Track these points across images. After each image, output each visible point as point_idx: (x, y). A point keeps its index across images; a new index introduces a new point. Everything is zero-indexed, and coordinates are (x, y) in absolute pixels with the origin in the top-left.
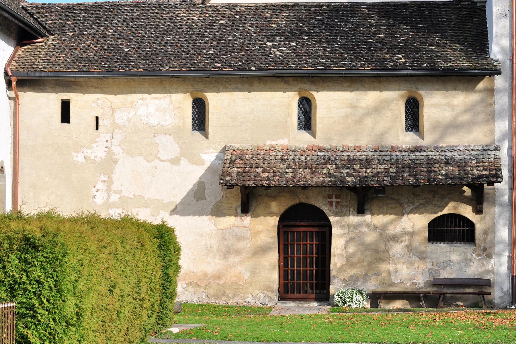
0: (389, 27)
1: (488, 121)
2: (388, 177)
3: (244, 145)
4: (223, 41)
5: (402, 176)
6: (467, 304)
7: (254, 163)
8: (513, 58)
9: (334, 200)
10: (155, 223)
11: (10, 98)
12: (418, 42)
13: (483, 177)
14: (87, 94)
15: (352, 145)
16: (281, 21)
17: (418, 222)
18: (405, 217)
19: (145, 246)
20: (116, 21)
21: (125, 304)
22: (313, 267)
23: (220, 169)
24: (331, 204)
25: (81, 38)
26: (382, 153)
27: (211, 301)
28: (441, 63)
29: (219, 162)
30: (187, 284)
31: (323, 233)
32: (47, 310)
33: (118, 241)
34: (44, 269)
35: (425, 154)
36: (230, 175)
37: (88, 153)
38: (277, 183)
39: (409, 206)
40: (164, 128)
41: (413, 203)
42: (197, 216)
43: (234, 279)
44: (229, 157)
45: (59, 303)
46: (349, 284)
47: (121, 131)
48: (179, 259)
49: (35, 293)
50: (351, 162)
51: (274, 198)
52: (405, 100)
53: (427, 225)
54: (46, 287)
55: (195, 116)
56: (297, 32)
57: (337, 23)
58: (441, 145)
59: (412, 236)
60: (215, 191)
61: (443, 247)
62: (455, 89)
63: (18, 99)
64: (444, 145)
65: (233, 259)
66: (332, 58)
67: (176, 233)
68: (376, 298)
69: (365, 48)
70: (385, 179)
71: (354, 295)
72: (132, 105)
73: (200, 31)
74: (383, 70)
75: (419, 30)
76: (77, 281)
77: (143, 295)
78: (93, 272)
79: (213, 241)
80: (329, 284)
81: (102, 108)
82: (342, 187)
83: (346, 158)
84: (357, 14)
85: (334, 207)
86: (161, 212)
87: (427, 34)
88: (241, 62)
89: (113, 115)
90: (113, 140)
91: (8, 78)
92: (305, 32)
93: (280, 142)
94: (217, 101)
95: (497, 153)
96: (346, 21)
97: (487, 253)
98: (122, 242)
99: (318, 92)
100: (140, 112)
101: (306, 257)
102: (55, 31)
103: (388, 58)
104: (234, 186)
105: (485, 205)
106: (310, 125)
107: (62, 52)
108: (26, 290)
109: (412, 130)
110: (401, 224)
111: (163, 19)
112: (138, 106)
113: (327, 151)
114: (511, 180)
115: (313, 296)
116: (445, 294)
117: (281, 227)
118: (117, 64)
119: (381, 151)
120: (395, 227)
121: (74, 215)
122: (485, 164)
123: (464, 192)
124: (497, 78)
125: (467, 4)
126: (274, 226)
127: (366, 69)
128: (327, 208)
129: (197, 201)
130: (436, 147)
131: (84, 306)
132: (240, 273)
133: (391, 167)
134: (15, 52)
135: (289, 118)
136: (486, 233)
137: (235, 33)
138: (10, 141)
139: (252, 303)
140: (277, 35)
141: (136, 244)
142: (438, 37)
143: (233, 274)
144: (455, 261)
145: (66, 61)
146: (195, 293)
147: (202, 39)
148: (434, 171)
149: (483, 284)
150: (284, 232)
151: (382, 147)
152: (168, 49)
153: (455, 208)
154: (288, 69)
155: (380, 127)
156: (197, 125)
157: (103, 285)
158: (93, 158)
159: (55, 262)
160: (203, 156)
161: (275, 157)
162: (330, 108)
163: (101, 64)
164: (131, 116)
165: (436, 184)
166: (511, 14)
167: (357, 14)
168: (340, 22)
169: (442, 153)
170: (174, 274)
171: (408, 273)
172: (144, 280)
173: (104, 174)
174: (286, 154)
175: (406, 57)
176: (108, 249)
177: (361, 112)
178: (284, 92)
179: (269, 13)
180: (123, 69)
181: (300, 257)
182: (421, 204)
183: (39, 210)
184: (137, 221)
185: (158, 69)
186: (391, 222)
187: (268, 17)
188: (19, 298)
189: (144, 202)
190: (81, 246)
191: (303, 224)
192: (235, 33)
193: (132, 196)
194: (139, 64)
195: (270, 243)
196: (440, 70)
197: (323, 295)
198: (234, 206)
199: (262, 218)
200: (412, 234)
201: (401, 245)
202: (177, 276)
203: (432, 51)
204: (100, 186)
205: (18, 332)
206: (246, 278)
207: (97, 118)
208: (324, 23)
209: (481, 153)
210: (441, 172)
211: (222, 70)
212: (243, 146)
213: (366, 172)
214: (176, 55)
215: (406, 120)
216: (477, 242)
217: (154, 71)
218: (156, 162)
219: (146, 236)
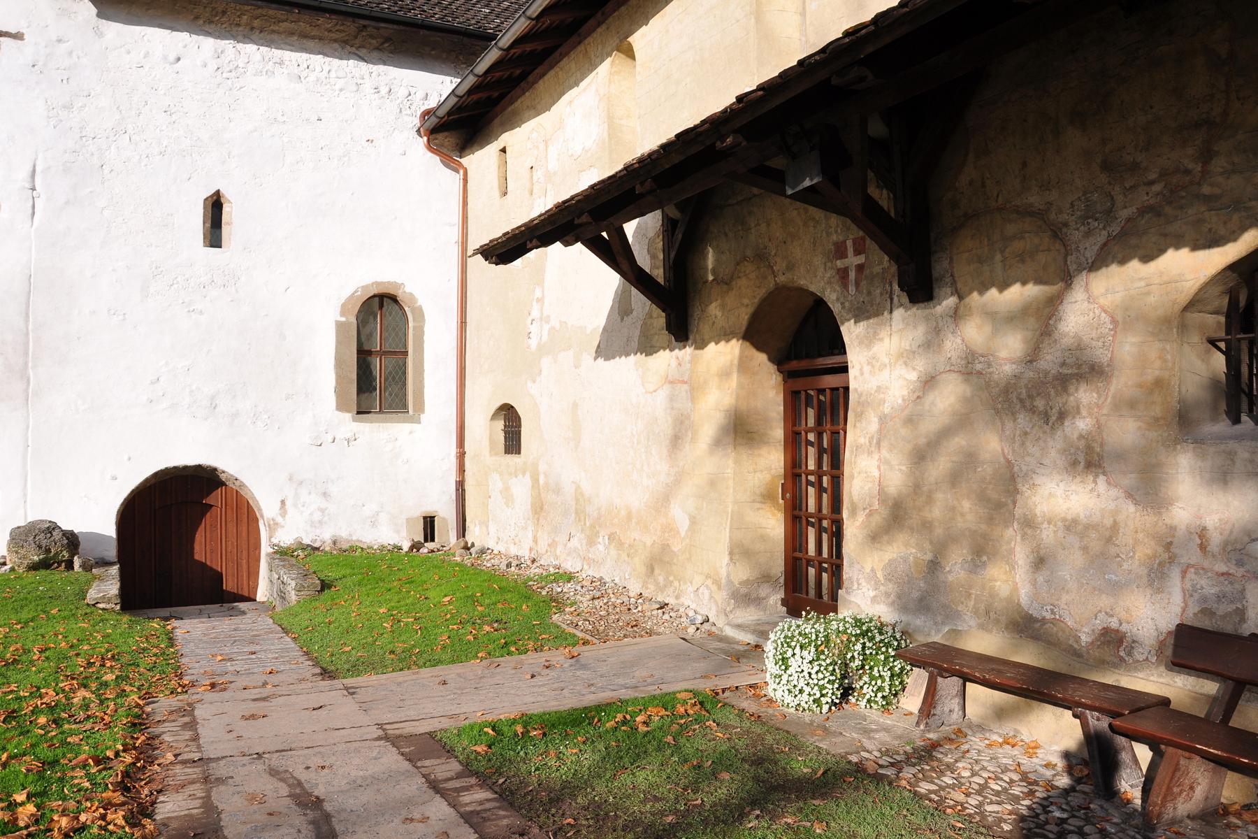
39: (1088, 234)
182: (1142, 211)
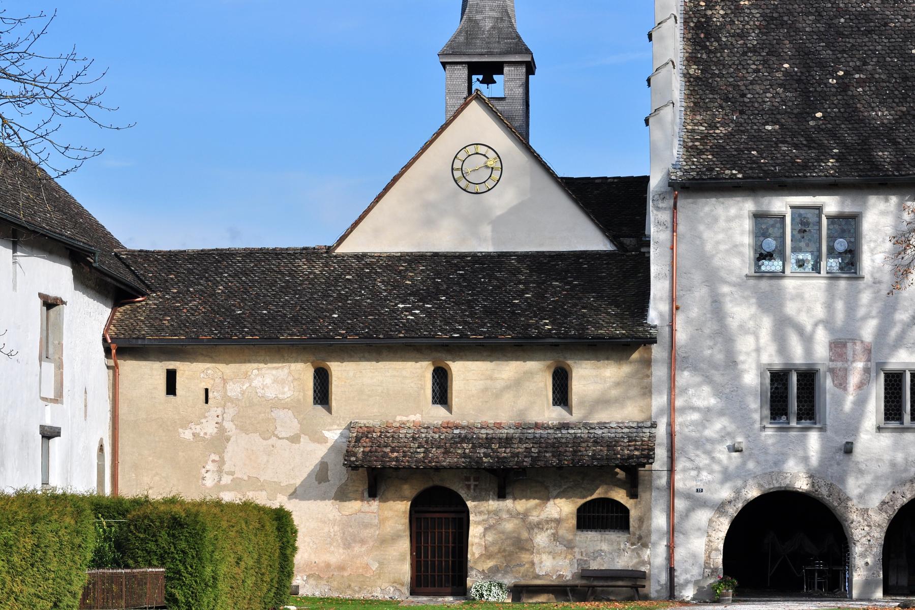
0: (539, 284)
1: (644, 394)
9: (472, 483)
11: (108, 367)
15: (492, 421)
17: (563, 508)
18: (551, 502)
23: (345, 448)
24: (468, 487)
26: (525, 431)
27: (335, 595)
28: (591, 330)
30: (308, 576)
31: (461, 519)
35: (573, 431)
36: (355, 454)
37: (197, 428)
41: (560, 486)
45: (200, 568)
50: (489, 440)
51: (405, 480)
52: (552, 370)
62: (608, 359)
65: (357, 549)
68: (519, 592)
72: (246, 376)
74: (525, 338)
77: (263, 570)
78: (225, 546)
82: (478, 468)
83: (484, 436)
85: (472, 491)
86: (279, 495)
87: (582, 293)
89: (224, 387)
91: (107, 345)
93: (412, 418)
94: (342, 372)
95: (653, 430)
97: (642, 541)
98: (246, 523)
103: (533, 324)
107: (166, 315)
108: (173, 558)
111: (280, 272)
112: (253, 376)
113: (463, 428)
116: (594, 587)
123: (617, 473)
124: (654, 346)
129: (320, 483)
130: (586, 424)
139: (380, 597)
140: (410, 295)
141: (257, 525)
144: (609, 552)
146: (317, 586)
151: (525, 424)
154: (420, 337)
155: (522, 403)
158: (202, 435)
160: (327, 434)
164: (244, 388)
165: (581, 466)
169: (591, 431)
171: (551, 564)
175: (552, 323)
184: (257, 505)
188: (168, 565)
193: (246, 478)
197: (459, 588)
198: (360, 489)
200: (558, 521)
203: (584, 315)
204: (210, 466)
207: (207, 390)
212: (371, 423)
213: (504, 453)
214: (295, 319)
215: (554, 392)
216: (631, 529)
219: (266, 517)
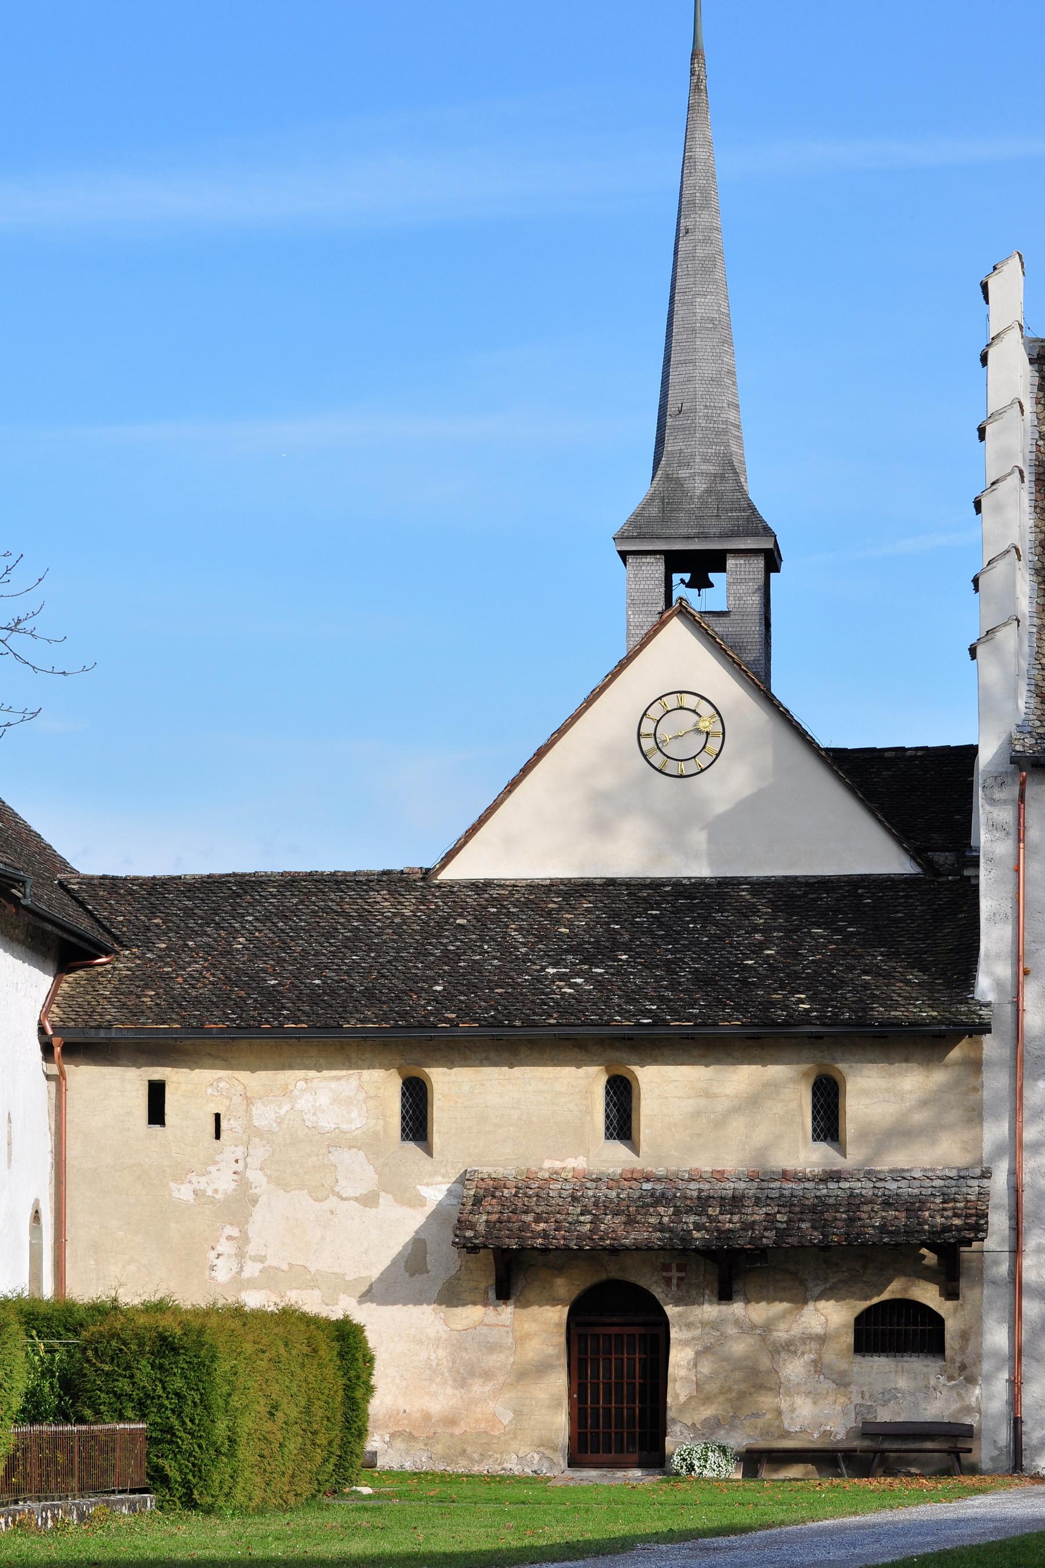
0: (789, 932)
2: (771, 1230)
3: (501, 1170)
4: (462, 964)
5: (799, 1228)
6: (932, 1469)
7: (520, 1204)
8: (1018, 1000)
9: (675, 1274)
10: (334, 1317)
11: (48, 1077)
12: (841, 965)
13: (950, 1231)
14: (197, 1070)
15: (709, 1169)
16: (575, 922)
17: (831, 1316)
18: (811, 1306)
19: (320, 1353)
20: (250, 918)
21: (290, 1435)
22: (634, 1403)
24: (668, 1281)
25: (183, 956)
26: (765, 1185)
27: (439, 1467)
28: (878, 1011)
29: (454, 1202)
30: (393, 1435)
32: (190, 1434)
33: (280, 1344)
34: (186, 1378)
36: (472, 1226)
37: (202, 1183)
38: (562, 1242)
39: (817, 1285)
40: (348, 1136)
41: (826, 1280)
42: (410, 1306)
43: (483, 1425)
44: (472, 1192)
45: (207, 1423)
46: (703, 1435)
47: (264, 1142)
48: (371, 1374)
49: (173, 1411)
50: (703, 1201)
51: (559, 1270)
52: (812, 1081)
53: (853, 1322)
54: (189, 1402)
55: (407, 1112)
56: (607, 944)
57: (689, 923)
58: (878, 1168)
59: (824, 1342)
60: (444, 1258)
61: (879, 1364)
62: (906, 1060)
63: (65, 1079)
64: (886, 1168)
65: (478, 1388)
66: (670, 1000)
67: (366, 1333)
68: (754, 1461)
69: (737, 980)
70: (766, 1234)
71: (710, 1454)
72: (286, 1091)
73: (417, 941)
74: (766, 1025)
75: (847, 938)
76: (230, 1395)
77: (315, 1427)
78: (249, 1384)
79: (441, 1353)
80: (665, 1435)
81: (227, 1097)
82: (684, 1250)
83: (695, 1194)
84: (729, 904)
86: (342, 1296)
87: (862, 947)
88: (496, 1009)
89: (248, 1110)
90: (249, 1159)
91: (46, 1040)
92: (623, 943)
94: (450, 1085)
95: (985, 1183)
96: (706, 920)
97: (967, 1374)
98: (286, 1345)
99: (642, 1066)
100: (301, 1104)
101: (622, 1384)
102: (131, 940)
103: (778, 1001)
104: (480, 1248)
105: (963, 1283)
106: (630, 1129)
107: (147, 987)
108: (162, 1406)
109: (824, 1140)
110: (803, 1319)
112: (296, 1092)
113: (659, 1180)
114: (1014, 1233)
115: (635, 1457)
117: (572, 1326)
118: (255, 1013)
119: (763, 1180)
120: (790, 1327)
121: (203, 1305)
122: (958, 1205)
123: (924, 1257)
124: (987, 1039)
125: (951, 881)
126: (557, 1325)
127: (733, 1022)
128: (660, 1290)
129: (412, 1275)
130: (869, 1172)
131: (238, 1429)
132: (494, 1415)
133: (779, 1212)
134: (56, 986)
135: (589, 1117)
136: (964, 1336)
137: (486, 947)
138: (49, 1160)
139: (517, 1470)
140: (567, 952)
141: (306, 1349)
142: (881, 955)
143: (480, 1416)
144: (908, 1391)
145: (157, 1004)
146: (407, 1452)
147: (421, 958)
148: (860, 1219)
149: (957, 1433)
150: (579, 1336)
151: (765, 1173)
152: (355, 980)
153: (905, 1290)
155: (760, 1136)
156: (411, 1130)
157: (262, 1403)
159: (202, 1369)
160: (424, 1191)
161: (560, 1193)
162: (666, 1098)
163: (225, 1013)
164: (283, 1112)
165: (862, 1244)
166: (1015, 915)
167: (729, 904)
168: (693, 921)
169: (879, 1184)
170: (363, 1399)
171: (812, 1413)
172: (318, 1403)
173: (231, 1224)
174: (581, 1186)
175: (811, 999)
176: (267, 1354)
177: (721, 1106)
178: (578, 1067)
179: (555, 902)
180: (268, 1022)
181: (610, 1384)
182: (840, 1281)
183: (145, 1297)
184: (304, 1315)
185: (335, 1024)
186: (783, 1316)
187: (553, 909)
188: (152, 1417)
189: (309, 1277)
190: (234, 1348)
191: (614, 1319)
192: (486, 947)
194: (299, 1014)
195: (551, 1356)
196: (874, 1025)
197: (653, 1457)
198: (483, 1285)
199: (535, 1309)
200: (822, 1339)
201: (802, 1360)
202: (368, 1402)
203: (866, 986)
204: (224, 1247)
205: (149, 1463)
206: (506, 1423)
207: (218, 1117)
208: (662, 923)
209: (953, 1183)
210: (874, 1219)
211: (457, 1026)
212: (499, 1172)
213: (730, 1222)
214: (369, 994)
215: (814, 1118)
216: (948, 1352)
217: (327, 1027)
218: (333, 1202)
219: (320, 1336)
